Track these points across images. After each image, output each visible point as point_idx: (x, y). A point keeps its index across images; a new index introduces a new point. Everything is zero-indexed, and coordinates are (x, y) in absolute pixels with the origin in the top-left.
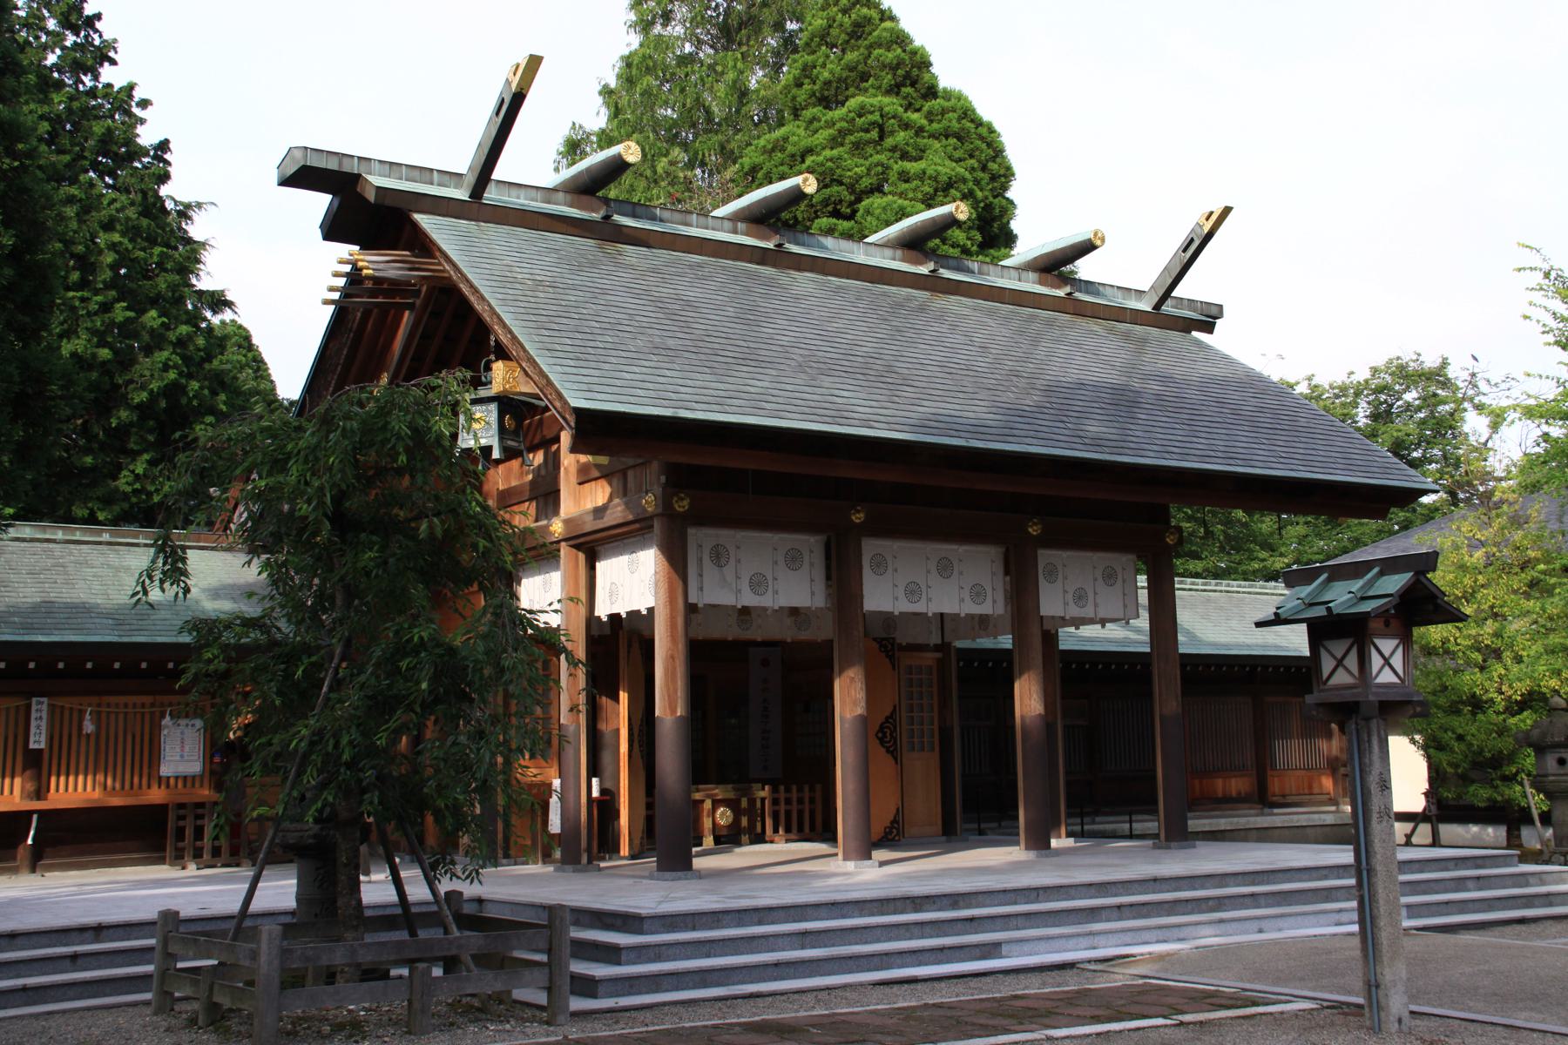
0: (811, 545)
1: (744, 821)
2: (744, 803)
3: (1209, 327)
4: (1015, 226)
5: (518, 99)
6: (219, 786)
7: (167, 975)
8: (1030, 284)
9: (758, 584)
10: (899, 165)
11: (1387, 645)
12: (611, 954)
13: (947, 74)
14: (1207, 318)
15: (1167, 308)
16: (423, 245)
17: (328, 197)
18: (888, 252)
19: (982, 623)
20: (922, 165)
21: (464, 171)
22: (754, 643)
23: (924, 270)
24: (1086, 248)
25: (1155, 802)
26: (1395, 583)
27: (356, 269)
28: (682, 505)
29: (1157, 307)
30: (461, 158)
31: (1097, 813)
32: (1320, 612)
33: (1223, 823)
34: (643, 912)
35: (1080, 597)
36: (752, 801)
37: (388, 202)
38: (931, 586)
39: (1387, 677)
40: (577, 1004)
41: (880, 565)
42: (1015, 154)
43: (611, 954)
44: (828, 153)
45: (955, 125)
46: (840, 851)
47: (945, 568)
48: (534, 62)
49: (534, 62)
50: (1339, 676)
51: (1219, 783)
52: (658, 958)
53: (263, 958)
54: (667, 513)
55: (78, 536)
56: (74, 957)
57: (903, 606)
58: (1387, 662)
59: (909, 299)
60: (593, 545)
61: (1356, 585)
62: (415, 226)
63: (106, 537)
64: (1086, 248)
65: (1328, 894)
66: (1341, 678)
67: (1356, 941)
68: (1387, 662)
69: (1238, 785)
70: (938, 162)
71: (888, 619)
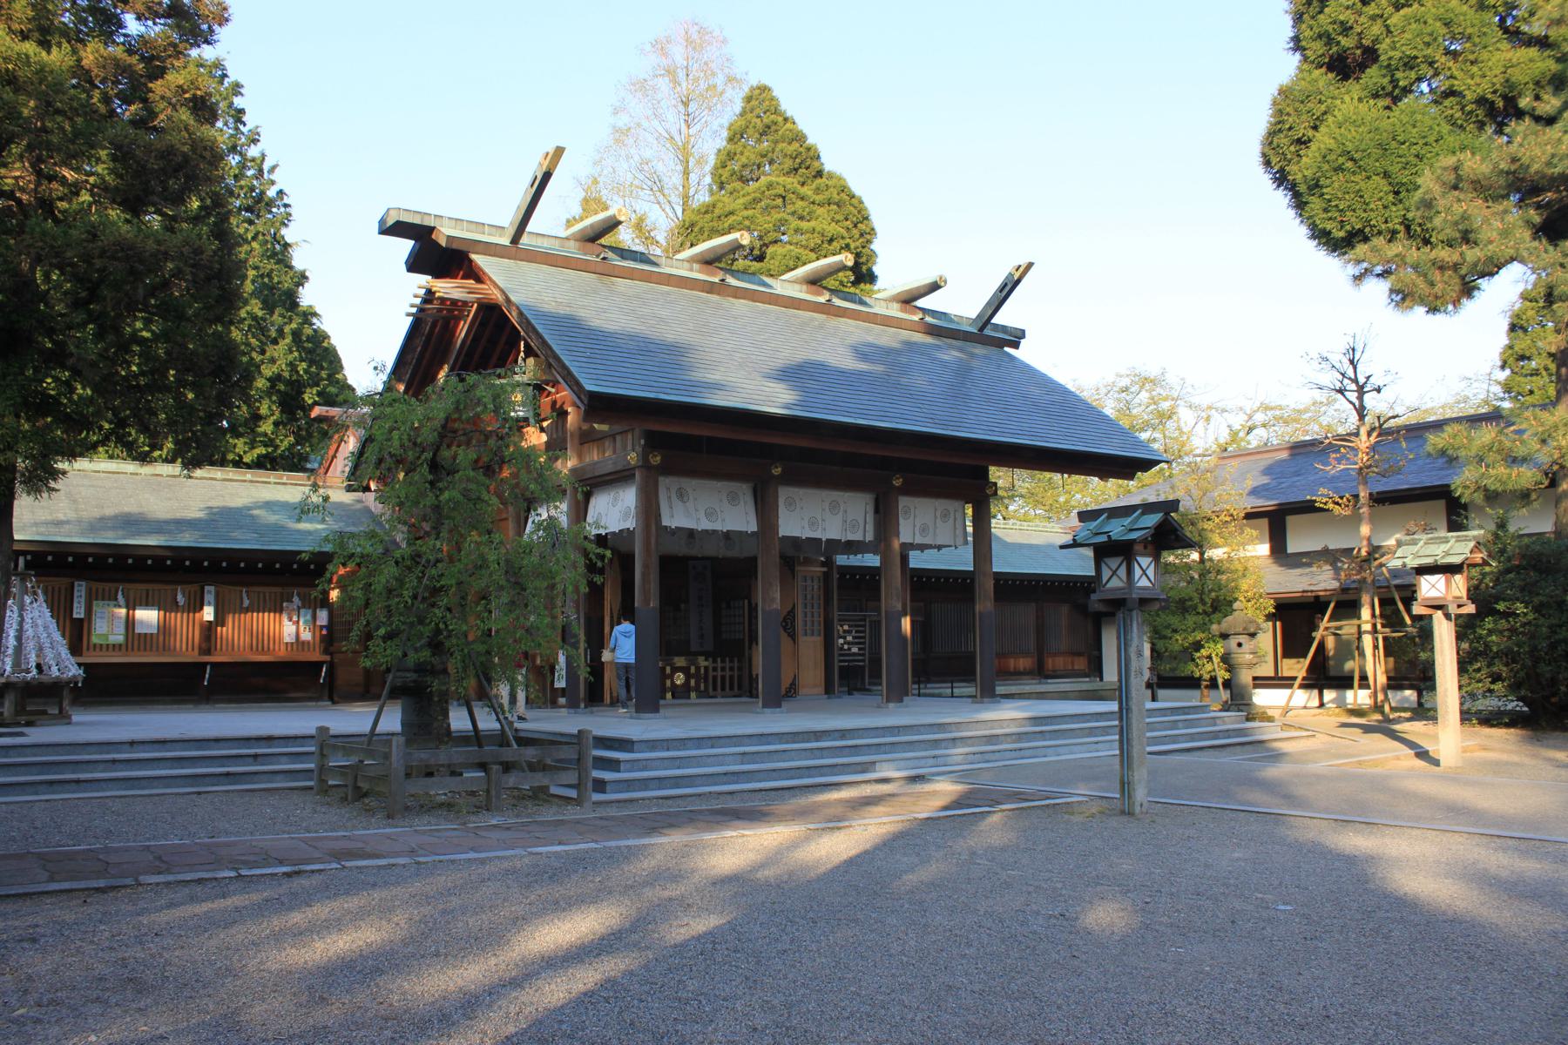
0: (744, 490)
1: (693, 682)
2: (693, 670)
3: (1016, 345)
4: (876, 270)
5: (547, 176)
6: (326, 651)
7: (322, 769)
8: (895, 311)
9: (710, 514)
10: (795, 223)
11: (1145, 561)
12: (613, 765)
13: (829, 163)
14: (1015, 338)
15: (987, 332)
16: (475, 274)
17: (411, 243)
18: (797, 287)
19: (851, 547)
20: (813, 223)
21: (506, 224)
22: (696, 558)
23: (822, 299)
24: (934, 287)
25: (974, 673)
26: (1152, 520)
27: (430, 292)
28: (656, 460)
29: (981, 329)
30: (507, 217)
31: (929, 681)
32: (1103, 538)
33: (1013, 689)
34: (635, 738)
35: (924, 530)
36: (698, 669)
37: (454, 246)
38: (820, 517)
39: (1144, 583)
40: (597, 797)
41: (791, 504)
42: (877, 220)
43: (613, 765)
44: (746, 213)
45: (836, 198)
46: (760, 701)
47: (834, 507)
48: (559, 151)
49: (559, 151)
50: (1114, 581)
51: (1012, 661)
52: (645, 769)
53: (394, 758)
54: (646, 465)
55: (231, 476)
56: (255, 756)
57: (806, 533)
58: (1144, 572)
59: (812, 320)
60: (589, 485)
61: (1127, 521)
62: (471, 261)
63: (249, 477)
64: (934, 287)
65: (1105, 731)
66: (1115, 583)
67: (1117, 760)
68: (1144, 572)
69: (1024, 663)
70: (824, 222)
71: (795, 542)
